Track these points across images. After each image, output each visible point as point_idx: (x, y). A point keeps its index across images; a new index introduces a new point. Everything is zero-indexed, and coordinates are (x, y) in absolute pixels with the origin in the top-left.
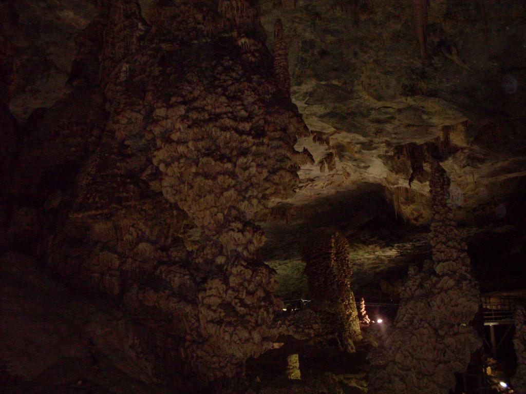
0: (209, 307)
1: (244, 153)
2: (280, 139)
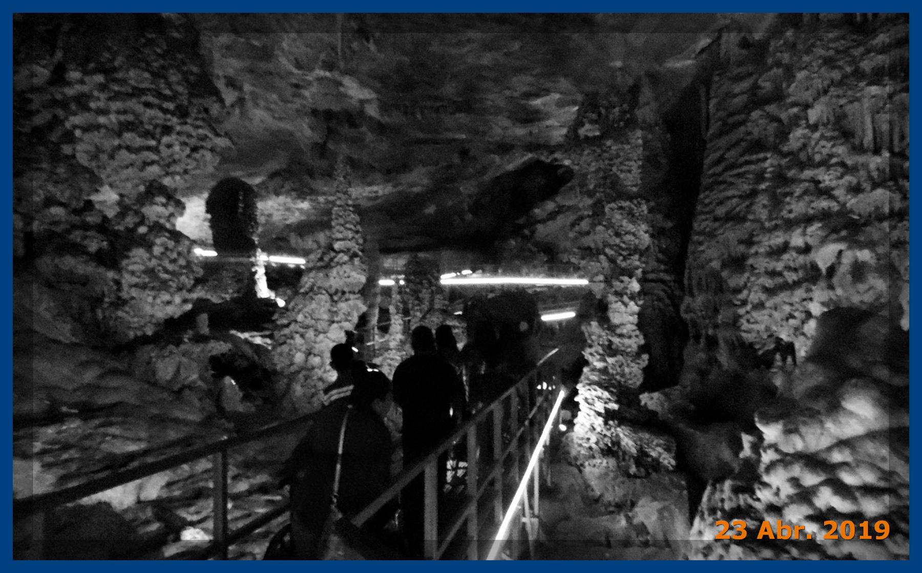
0: (133, 273)
1: (167, 130)
2: (203, 119)
